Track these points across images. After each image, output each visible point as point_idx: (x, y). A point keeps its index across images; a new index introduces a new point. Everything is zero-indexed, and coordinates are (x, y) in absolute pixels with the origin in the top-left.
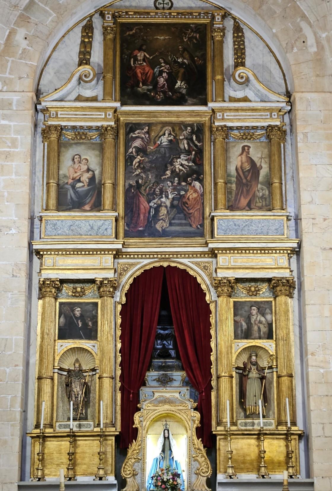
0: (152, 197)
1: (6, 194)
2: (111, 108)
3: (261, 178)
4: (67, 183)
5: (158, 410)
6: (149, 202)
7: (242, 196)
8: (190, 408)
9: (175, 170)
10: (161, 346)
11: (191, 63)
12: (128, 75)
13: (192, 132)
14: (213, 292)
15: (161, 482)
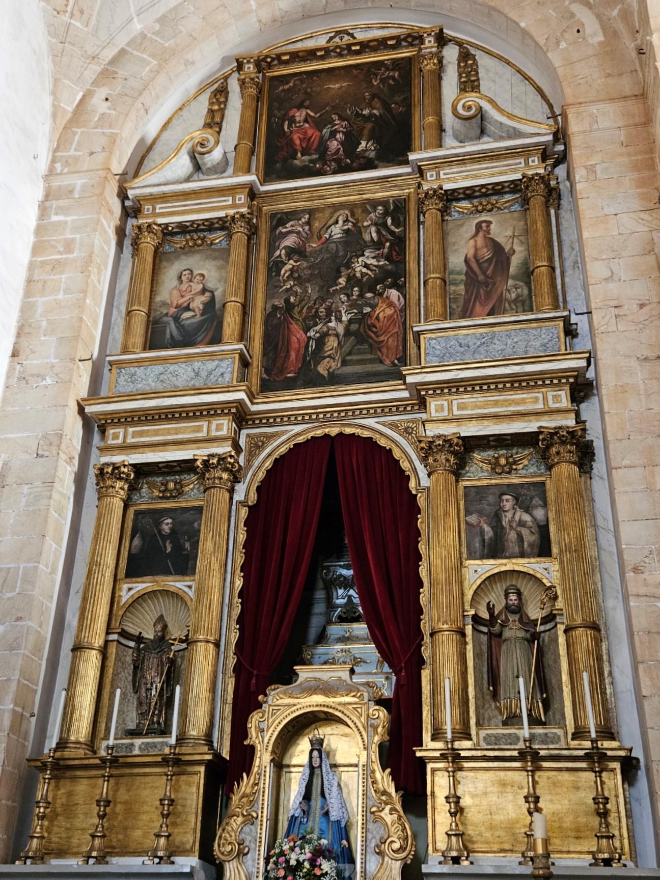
0: (312, 322)
1: (44, 324)
2: (241, 186)
3: (513, 270)
4: (167, 314)
5: (298, 706)
6: (307, 329)
7: (477, 303)
8: (366, 700)
9: (355, 275)
10: (345, 600)
11: (384, 113)
12: (279, 144)
13: (386, 213)
14: (422, 472)
15: (284, 868)
